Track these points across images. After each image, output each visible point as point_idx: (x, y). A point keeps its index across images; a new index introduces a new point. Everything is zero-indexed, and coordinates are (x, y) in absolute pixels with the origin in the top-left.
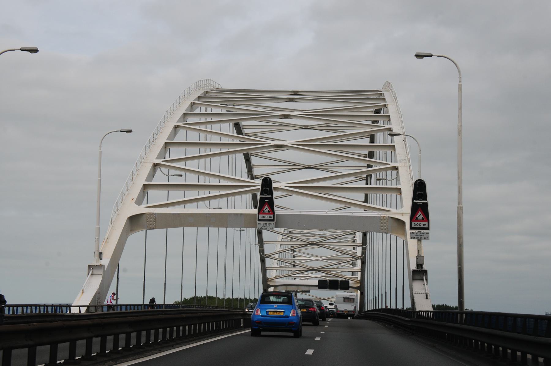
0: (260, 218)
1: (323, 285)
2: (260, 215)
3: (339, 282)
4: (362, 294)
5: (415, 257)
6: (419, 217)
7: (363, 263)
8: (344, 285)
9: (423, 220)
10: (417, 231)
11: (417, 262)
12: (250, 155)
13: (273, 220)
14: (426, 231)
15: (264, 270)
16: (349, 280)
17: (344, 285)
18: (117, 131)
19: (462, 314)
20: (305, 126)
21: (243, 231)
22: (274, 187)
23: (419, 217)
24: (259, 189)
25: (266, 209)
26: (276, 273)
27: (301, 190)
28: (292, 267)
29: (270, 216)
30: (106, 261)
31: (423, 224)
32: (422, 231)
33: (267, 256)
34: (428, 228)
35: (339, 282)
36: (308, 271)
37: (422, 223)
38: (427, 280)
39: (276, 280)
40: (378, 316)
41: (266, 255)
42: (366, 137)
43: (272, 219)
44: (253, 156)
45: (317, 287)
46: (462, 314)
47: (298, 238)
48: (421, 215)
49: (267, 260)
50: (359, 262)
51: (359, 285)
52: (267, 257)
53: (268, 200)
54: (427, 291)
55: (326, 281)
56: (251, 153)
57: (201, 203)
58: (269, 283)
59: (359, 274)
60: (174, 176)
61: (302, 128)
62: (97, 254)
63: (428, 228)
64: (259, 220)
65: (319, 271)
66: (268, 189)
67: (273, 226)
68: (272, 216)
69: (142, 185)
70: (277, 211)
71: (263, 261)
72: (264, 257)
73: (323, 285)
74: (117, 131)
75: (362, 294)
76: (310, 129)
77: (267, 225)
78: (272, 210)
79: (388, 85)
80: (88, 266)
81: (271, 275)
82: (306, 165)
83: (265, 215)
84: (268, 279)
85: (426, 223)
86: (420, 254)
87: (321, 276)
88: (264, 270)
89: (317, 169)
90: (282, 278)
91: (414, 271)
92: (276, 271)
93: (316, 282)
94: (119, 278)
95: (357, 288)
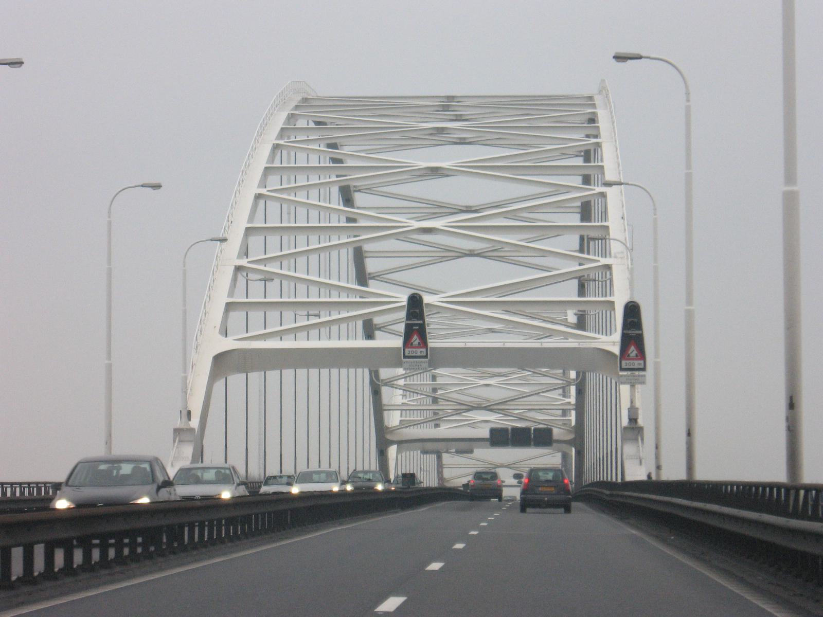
0: (406, 354)
1: (499, 438)
2: (407, 350)
3: (532, 432)
4: (580, 454)
5: (627, 409)
6: (631, 353)
7: (580, 392)
8: (542, 437)
9: (636, 358)
10: (629, 373)
11: (629, 416)
12: (352, 189)
13: (426, 357)
14: (641, 373)
15: (379, 409)
16: (553, 428)
17: (542, 437)
18: (136, 186)
19: (797, 490)
20: (467, 207)
21: (156, 191)
22: (425, 304)
23: (631, 353)
24: (404, 306)
25: (416, 340)
26: (401, 416)
27: (461, 306)
28: (431, 403)
29: (420, 351)
30: (195, 423)
31: (637, 364)
32: (637, 373)
33: (384, 382)
34: (644, 369)
35: (532, 432)
36: (468, 410)
37: (636, 362)
38: (642, 439)
39: (404, 429)
40: (643, 504)
41: (382, 380)
42: (577, 156)
43: (425, 354)
44: (359, 191)
45: (488, 443)
46: (797, 490)
47: (378, 191)
48: (634, 351)
49: (385, 390)
50: (573, 389)
51: (572, 436)
52: (386, 385)
53: (417, 328)
54: (641, 454)
55: (506, 430)
56: (354, 186)
57: (314, 333)
58: (389, 437)
59: (573, 413)
60: (142, 186)
61: (455, 143)
62: (185, 413)
63: (644, 369)
64: (405, 357)
65: (491, 410)
66: (417, 311)
67: (427, 365)
68: (424, 350)
69: (224, 305)
70: (432, 343)
71: (376, 393)
72: (379, 385)
73: (499, 438)
74: (206, 240)
75: (580, 454)
76: (470, 143)
77: (418, 364)
78: (424, 342)
79: (602, 90)
80: (172, 430)
81: (393, 419)
82: (466, 250)
83: (414, 350)
84: (387, 428)
85: (642, 362)
86: (633, 404)
87: (496, 419)
88: (379, 409)
89: (485, 257)
90: (415, 426)
91: (625, 428)
92: (400, 411)
93: (485, 433)
94: (228, 446)
95: (569, 443)
